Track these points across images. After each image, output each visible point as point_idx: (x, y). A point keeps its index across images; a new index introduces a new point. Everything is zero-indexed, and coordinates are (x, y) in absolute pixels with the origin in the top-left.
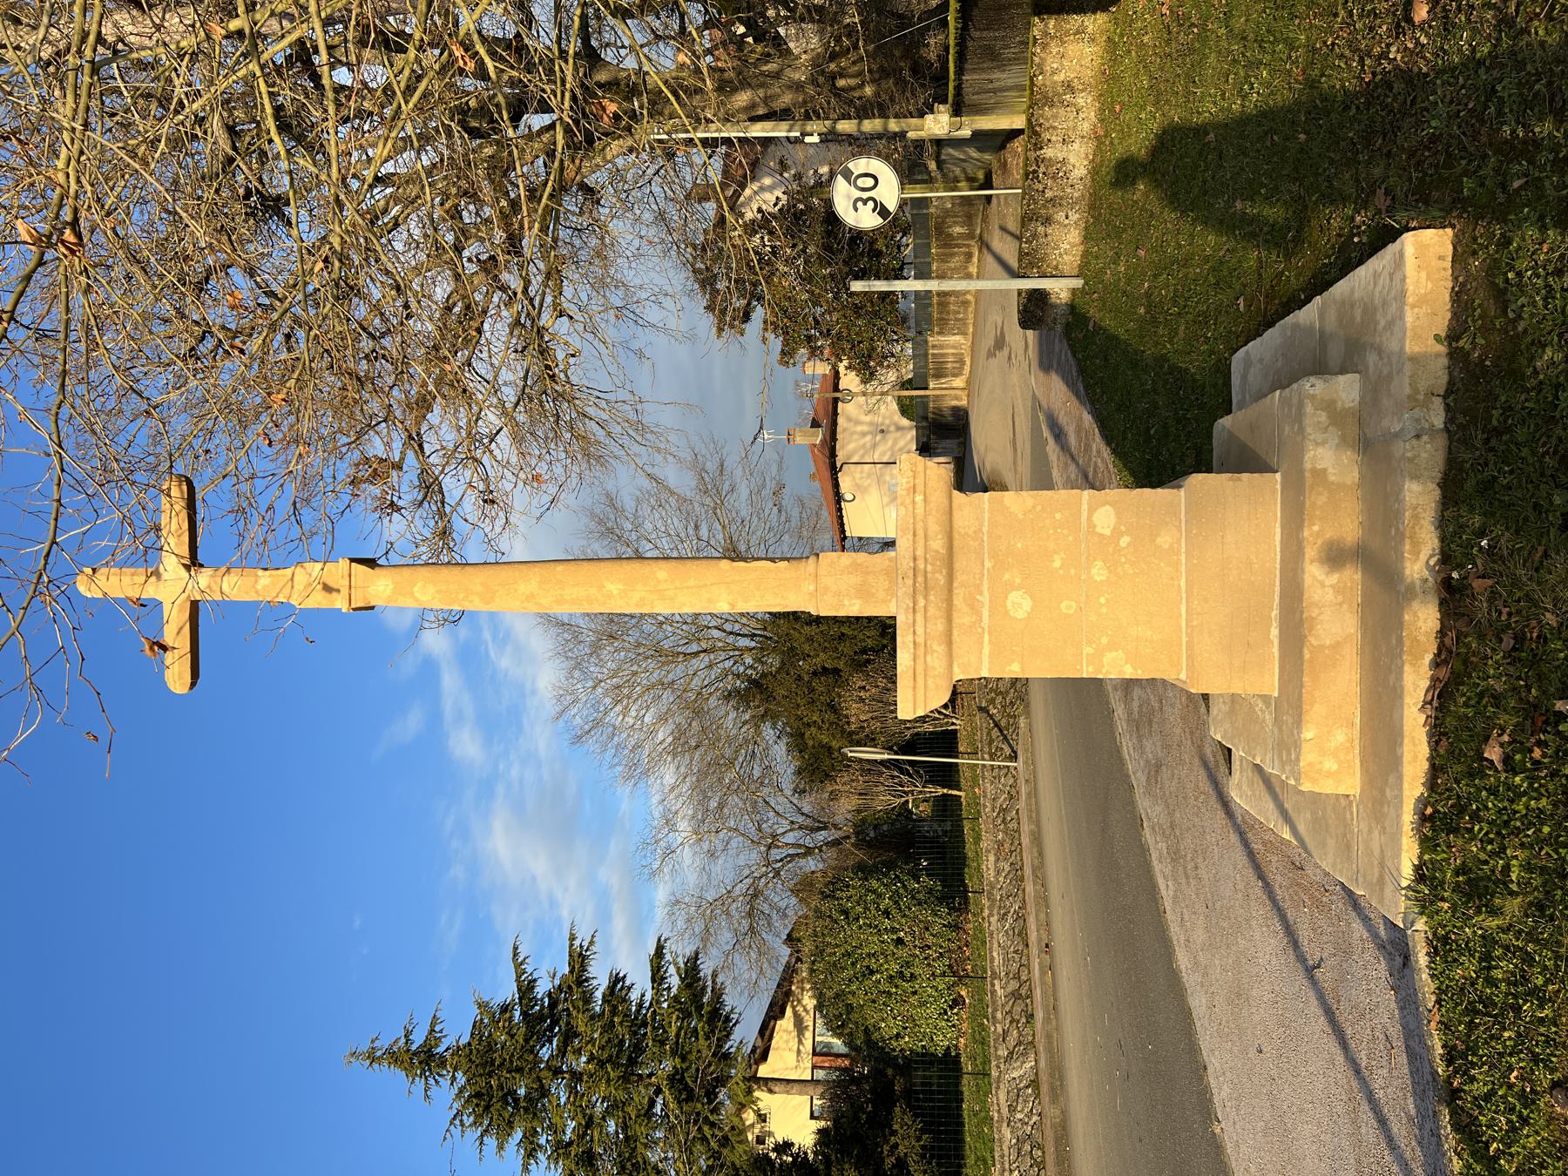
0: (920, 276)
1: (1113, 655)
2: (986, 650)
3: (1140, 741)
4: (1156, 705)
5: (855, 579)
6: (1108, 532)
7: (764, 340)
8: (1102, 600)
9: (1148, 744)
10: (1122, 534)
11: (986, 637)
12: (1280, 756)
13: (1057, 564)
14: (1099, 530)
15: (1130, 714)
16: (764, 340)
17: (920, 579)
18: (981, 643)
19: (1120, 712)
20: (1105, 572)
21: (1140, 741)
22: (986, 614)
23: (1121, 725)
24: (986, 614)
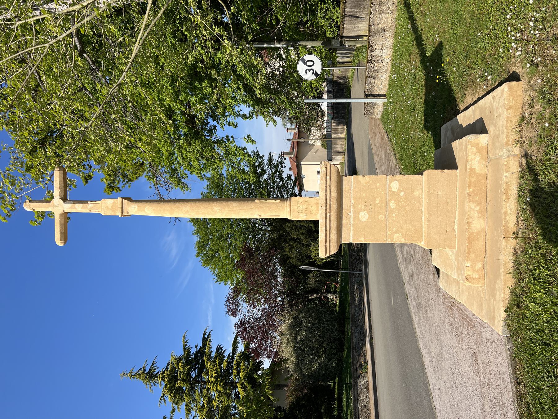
3: (406, 266)
6: (396, 190)
8: (394, 215)
9: (409, 267)
10: (401, 191)
12: (458, 272)
13: (378, 202)
14: (393, 190)
15: (403, 255)
17: (328, 207)
19: (399, 254)
21: (406, 266)
22: (352, 220)
23: (400, 259)
24: (352, 220)
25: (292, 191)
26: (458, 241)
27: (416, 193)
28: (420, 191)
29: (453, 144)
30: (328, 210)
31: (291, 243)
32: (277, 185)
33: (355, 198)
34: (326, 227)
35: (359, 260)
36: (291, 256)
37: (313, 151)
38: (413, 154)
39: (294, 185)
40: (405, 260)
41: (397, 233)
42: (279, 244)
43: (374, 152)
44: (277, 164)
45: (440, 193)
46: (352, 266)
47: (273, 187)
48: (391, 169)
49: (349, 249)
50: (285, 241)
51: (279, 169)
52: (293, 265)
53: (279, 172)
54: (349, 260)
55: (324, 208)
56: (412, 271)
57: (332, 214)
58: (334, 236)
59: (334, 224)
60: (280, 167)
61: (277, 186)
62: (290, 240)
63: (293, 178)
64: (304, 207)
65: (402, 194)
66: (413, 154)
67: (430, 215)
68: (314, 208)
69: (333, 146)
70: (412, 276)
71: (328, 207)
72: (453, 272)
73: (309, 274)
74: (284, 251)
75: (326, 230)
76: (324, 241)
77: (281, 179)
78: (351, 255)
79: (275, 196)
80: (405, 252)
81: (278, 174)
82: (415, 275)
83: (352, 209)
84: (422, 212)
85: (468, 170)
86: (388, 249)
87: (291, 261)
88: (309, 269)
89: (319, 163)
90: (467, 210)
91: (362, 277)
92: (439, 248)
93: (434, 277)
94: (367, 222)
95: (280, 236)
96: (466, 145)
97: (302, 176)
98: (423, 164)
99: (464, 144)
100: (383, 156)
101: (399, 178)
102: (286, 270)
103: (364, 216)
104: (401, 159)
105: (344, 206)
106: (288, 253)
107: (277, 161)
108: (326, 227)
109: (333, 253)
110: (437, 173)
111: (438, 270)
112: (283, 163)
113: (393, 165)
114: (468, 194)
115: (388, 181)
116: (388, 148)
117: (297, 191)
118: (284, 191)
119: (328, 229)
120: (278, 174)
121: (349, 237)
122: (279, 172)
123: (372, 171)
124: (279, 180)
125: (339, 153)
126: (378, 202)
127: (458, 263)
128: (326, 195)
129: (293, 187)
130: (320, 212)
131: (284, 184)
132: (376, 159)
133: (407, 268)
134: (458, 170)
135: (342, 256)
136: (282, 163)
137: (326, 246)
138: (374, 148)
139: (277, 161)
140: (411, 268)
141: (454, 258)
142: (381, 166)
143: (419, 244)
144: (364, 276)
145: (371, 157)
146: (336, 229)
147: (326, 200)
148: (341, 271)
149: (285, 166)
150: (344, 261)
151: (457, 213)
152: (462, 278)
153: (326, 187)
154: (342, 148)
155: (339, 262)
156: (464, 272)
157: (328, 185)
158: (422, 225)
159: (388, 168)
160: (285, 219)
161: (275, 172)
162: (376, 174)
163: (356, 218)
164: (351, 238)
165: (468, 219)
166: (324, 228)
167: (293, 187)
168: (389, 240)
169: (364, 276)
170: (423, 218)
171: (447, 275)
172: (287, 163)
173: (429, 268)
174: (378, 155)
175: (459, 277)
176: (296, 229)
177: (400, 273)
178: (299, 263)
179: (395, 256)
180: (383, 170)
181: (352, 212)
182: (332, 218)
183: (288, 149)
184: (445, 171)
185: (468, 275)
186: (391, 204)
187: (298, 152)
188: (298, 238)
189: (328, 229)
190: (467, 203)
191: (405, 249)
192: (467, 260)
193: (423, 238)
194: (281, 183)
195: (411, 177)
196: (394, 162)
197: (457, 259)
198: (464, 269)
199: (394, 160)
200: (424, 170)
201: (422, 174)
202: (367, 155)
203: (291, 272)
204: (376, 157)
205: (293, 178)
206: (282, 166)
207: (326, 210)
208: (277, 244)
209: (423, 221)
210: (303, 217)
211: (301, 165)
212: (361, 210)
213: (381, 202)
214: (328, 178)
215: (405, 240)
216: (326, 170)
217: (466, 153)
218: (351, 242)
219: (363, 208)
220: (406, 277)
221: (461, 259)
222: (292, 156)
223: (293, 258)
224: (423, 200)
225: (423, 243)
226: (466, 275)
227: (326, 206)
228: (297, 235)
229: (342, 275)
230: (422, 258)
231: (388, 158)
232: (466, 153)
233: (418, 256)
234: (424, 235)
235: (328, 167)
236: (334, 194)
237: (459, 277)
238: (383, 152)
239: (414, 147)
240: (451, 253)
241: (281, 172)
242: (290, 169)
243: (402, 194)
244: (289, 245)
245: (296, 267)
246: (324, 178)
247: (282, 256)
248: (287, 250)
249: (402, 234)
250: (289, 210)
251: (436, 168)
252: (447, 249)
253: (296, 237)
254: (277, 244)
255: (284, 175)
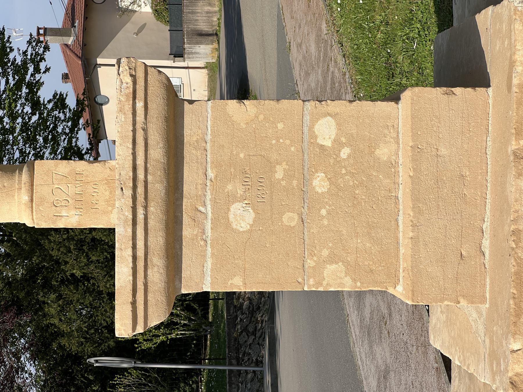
0: (240, 371)
1: (334, 267)
2: (209, 264)
3: (371, 347)
4: (385, 311)
5: (72, 190)
6: (328, 143)
7: (67, 95)
8: (324, 212)
9: (378, 350)
10: (342, 145)
11: (209, 249)
12: (491, 365)
13: (279, 174)
14: (320, 141)
15: (362, 320)
16: (67, 95)
17: (140, 190)
18: (204, 256)
19: (353, 318)
20: (327, 184)
21: (371, 347)
22: (208, 226)
23: (355, 331)
24: (208, 226)
25: (70, 142)
26: (492, 283)
27: (383, 152)
28: (394, 147)
29: (480, 18)
30: (140, 198)
31: (64, 291)
32: (25, 125)
33: (217, 165)
34: (134, 247)
35: (254, 333)
36: (64, 327)
37: (130, 28)
38: (386, 43)
39: (75, 124)
40: (368, 331)
41: (332, 262)
42: (28, 294)
43: (290, 36)
44: (25, 63)
45: (443, 151)
46: (238, 350)
47: (12, 130)
48: (333, 83)
49: (229, 304)
50: (47, 286)
51: (28, 77)
52: (69, 355)
53: (30, 85)
54: (229, 335)
55: (129, 193)
56: (385, 362)
57: (151, 209)
58: (157, 275)
59: (158, 240)
60: (31, 70)
61: (25, 127)
62: (62, 282)
63: (71, 102)
64: (72, 190)
65: (345, 153)
66: (386, 43)
67: (418, 211)
68: (103, 192)
69: (185, 17)
70: (384, 375)
71: (140, 190)
72: (481, 366)
73: (117, 380)
74: (45, 316)
75: (135, 258)
76: (130, 287)
77: (36, 105)
78: (232, 322)
79: (17, 155)
80: (367, 315)
81: (25, 90)
82: (392, 374)
83: (209, 197)
84: (397, 203)
85: (515, 89)
86: (328, 303)
87: (64, 341)
88: (115, 365)
89: (114, 61)
90: (512, 198)
91: (261, 381)
92: (442, 300)
93: (439, 378)
94: (250, 231)
95: (33, 273)
96: (511, 22)
97: (99, 100)
98: (411, 72)
99: (505, 17)
100: (313, 49)
101: (338, 110)
102: (48, 371)
103: (242, 217)
104: (357, 58)
105: (188, 188)
106: (56, 321)
107: (25, 53)
108: (134, 247)
109: (154, 322)
110: (437, 93)
111: (447, 362)
112: (42, 59)
113: (337, 74)
114: (515, 153)
115: (307, 118)
116: (324, 26)
117: (83, 140)
118: (46, 140)
119: (140, 253)
120: (25, 90)
121: (202, 277)
122: (30, 85)
123: (287, 91)
124: (28, 109)
125: (202, 36)
126: (279, 174)
127: (492, 341)
128: (134, 154)
129: (72, 130)
130: (117, 204)
131: (43, 121)
132: (295, 56)
133: (372, 354)
134: (490, 90)
135: (211, 324)
136: (37, 60)
137: (134, 304)
138: (289, 24)
139: (25, 53)
140: (383, 352)
141: (481, 328)
142: (307, 74)
143: (391, 291)
144: (268, 379)
145: (283, 49)
146: (162, 253)
147: (135, 168)
148: (205, 367)
149: (47, 70)
150: (216, 336)
151: (488, 206)
152: (501, 382)
153: (134, 131)
154: (210, 23)
155: (201, 340)
156: (507, 366)
157: (139, 126)
158: (397, 238)
159: (325, 82)
160: (16, 224)
161: (18, 86)
162: (294, 95)
163: (222, 220)
164: (208, 279)
165: (515, 221)
166: (130, 252)
167: (72, 130)
168: (312, 281)
169: (268, 379)
170: (401, 218)
171: (471, 377)
172: (56, 60)
173: (425, 353)
174: (300, 45)
175: (494, 380)
176: (80, 249)
177: (354, 368)
178: (89, 348)
179: (344, 322)
180: (313, 85)
181: (208, 203)
182: (151, 223)
183: (56, 19)
184: (458, 90)
185: (517, 375)
186: (316, 183)
187: (85, 30)
188: (86, 277)
189: (140, 253)
190: (511, 178)
191: (367, 304)
192: (514, 334)
193: (401, 275)
194: (35, 118)
195: (367, 105)
196: (339, 66)
197: (488, 330)
198: (505, 357)
199: (341, 61)
200: (404, 88)
201: (396, 99)
202: (274, 45)
203: (65, 373)
204: (294, 48)
205: (71, 102)
206: (37, 70)
207: (134, 198)
208: (22, 295)
209: (401, 228)
210: (71, 219)
211: (97, 66)
212: (232, 199)
213: (288, 176)
214: (140, 105)
215: (355, 280)
216: (135, 83)
217: (510, 44)
218: (207, 288)
219: (240, 192)
220: (371, 379)
221: (500, 332)
222: (70, 41)
223: (70, 335)
224: (401, 169)
225: (400, 288)
226: (510, 374)
227: (135, 187)
228: (81, 268)
229: (209, 376)
230: (409, 325)
231: (326, 54)
232: (510, 44)
233: (399, 322)
234: (402, 265)
235: (140, 75)
236: (158, 153)
237: (494, 380)
238: (313, 37)
239: (387, 24)
240: (475, 315)
241: (34, 87)
242: (65, 77)
243: (345, 153)
244: (60, 297)
245: (78, 359)
246: (128, 107)
247: (38, 327)
248: (53, 311)
249: (347, 264)
250: (25, 198)
251: (437, 84)
252: (463, 303)
253: (78, 273)
254: (22, 295)
255: (45, 94)
